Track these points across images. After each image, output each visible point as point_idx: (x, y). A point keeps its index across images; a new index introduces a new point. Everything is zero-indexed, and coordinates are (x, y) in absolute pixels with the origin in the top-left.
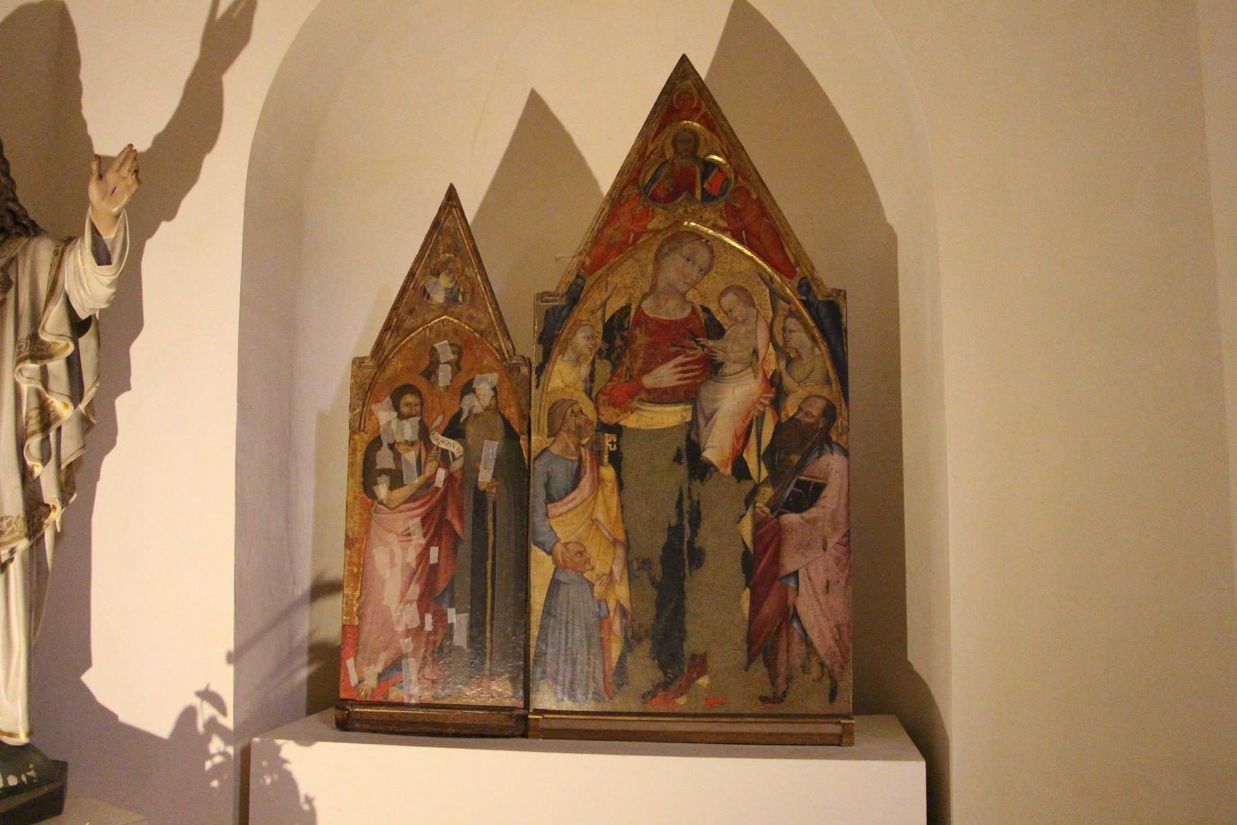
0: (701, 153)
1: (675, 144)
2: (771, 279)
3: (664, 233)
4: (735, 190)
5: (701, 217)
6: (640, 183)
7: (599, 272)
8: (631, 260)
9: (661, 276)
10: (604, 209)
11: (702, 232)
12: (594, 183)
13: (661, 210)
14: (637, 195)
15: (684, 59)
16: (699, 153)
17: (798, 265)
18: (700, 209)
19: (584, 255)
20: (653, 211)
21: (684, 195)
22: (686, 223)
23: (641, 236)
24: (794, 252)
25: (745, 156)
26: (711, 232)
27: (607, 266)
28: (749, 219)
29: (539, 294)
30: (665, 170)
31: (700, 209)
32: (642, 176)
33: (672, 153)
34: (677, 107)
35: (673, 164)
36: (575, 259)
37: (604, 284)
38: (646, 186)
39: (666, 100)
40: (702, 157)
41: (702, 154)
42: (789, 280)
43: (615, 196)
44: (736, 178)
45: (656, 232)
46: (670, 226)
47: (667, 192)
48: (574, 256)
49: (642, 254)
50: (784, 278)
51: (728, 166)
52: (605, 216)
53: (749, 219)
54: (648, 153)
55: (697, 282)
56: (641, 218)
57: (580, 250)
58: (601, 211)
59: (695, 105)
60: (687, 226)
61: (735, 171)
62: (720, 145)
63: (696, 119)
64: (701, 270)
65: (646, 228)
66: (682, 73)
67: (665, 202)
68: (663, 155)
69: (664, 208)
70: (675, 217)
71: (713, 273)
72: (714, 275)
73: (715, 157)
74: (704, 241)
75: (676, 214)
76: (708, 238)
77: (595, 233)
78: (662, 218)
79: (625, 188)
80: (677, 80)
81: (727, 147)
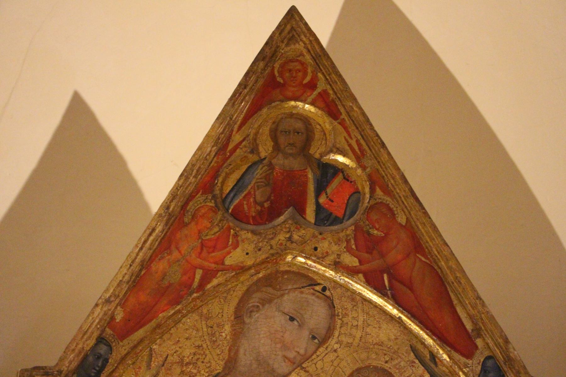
0: (316, 151)
1: (274, 135)
2: (433, 357)
3: (253, 271)
4: (371, 208)
5: (316, 249)
6: (217, 192)
7: (140, 333)
8: (195, 316)
9: (245, 346)
10: (154, 230)
11: (317, 273)
12: (145, 205)
13: (250, 235)
14: (211, 209)
15: (293, 13)
16: (312, 151)
17: (479, 335)
18: (314, 236)
19: (113, 305)
20: (236, 236)
21: (289, 211)
22: (289, 258)
23: (214, 276)
24: (472, 312)
25: (386, 156)
26: (330, 273)
27: (153, 323)
28: (394, 256)
29: (26, 370)
30: (259, 172)
31: (314, 236)
32: (220, 179)
33: (271, 149)
34: (279, 80)
35: (271, 166)
36: (98, 310)
37: (146, 353)
38: (226, 197)
39: (264, 69)
40: (317, 156)
41: (319, 151)
42: (463, 360)
43: (173, 211)
44: (372, 190)
45: (241, 269)
46: (263, 262)
47: (259, 208)
48: (97, 305)
49: (214, 307)
50: (457, 356)
51: (359, 171)
52: (155, 240)
53: (394, 256)
54: (230, 147)
55: (307, 358)
56: (215, 247)
57: (108, 295)
58: (148, 232)
59: (308, 79)
60: (290, 264)
61: (370, 178)
62: (346, 140)
63: (309, 100)
64: (314, 338)
65: (223, 263)
66: (289, 33)
67: (256, 223)
68: (254, 150)
69: (253, 232)
70: (272, 248)
71: (332, 343)
72: (336, 346)
73: (340, 159)
74: (318, 288)
75: (273, 242)
76: (327, 284)
77: (136, 267)
78: (250, 248)
79: (191, 197)
80: (282, 42)
81: (357, 141)
